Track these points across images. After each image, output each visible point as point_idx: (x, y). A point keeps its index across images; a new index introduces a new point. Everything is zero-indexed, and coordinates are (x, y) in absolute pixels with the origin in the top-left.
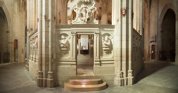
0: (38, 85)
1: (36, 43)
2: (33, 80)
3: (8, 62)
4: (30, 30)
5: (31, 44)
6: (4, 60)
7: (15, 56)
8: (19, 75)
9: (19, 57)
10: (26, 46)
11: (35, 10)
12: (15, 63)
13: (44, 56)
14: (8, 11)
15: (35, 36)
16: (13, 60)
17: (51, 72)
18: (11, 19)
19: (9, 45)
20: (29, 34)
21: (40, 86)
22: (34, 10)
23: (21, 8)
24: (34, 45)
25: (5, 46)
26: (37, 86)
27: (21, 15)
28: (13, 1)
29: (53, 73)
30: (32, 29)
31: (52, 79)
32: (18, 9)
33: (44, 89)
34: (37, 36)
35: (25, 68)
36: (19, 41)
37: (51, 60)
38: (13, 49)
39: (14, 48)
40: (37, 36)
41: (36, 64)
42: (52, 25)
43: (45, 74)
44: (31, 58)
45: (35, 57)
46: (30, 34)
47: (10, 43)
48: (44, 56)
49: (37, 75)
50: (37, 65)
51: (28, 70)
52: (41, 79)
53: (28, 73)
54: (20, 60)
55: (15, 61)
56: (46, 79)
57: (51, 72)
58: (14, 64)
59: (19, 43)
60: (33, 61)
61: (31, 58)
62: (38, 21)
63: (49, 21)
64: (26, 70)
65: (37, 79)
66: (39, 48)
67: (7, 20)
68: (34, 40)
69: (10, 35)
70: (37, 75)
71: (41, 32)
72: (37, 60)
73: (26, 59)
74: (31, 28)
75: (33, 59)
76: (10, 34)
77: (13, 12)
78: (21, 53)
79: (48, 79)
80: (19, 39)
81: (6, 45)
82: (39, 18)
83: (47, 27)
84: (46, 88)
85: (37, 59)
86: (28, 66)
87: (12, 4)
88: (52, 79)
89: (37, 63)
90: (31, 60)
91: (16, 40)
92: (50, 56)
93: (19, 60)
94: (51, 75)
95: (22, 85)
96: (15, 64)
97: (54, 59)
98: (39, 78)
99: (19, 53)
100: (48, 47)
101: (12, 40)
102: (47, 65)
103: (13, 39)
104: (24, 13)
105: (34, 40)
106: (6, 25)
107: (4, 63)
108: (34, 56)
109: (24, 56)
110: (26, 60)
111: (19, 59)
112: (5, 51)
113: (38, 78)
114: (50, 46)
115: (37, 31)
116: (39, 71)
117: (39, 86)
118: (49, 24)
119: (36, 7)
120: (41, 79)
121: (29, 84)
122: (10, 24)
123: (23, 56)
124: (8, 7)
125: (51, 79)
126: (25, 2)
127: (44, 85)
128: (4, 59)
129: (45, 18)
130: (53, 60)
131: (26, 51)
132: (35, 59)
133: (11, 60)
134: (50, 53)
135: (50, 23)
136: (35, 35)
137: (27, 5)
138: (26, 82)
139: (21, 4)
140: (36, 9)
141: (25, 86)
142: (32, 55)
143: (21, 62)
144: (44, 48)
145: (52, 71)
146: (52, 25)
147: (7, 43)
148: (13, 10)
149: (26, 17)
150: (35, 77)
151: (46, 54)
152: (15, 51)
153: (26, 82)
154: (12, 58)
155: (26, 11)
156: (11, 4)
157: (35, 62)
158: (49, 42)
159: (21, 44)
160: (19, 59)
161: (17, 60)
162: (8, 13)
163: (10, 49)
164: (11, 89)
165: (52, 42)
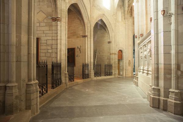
0: (152, 106)
1: (148, 50)
2: (144, 98)
3: (95, 74)
4: (140, 37)
5: (142, 53)
6: (105, 73)
7: (119, 69)
8: (124, 90)
9: (124, 70)
10: (134, 57)
11: (147, 11)
12: (119, 76)
13: (161, 66)
14: (109, 21)
15: (147, 41)
16: (117, 72)
17: (177, 91)
18: (113, 29)
19: (111, 57)
20: (137, 41)
21: (156, 108)
22: (144, 11)
23: (126, 15)
24: (145, 53)
25: (106, 58)
26: (150, 106)
27: (127, 22)
28: (115, 11)
29: (181, 93)
30: (142, 35)
31: (178, 102)
32: (122, 17)
33: (162, 112)
34: (151, 40)
35: (132, 83)
36: (124, 52)
37: (176, 73)
38: (117, 60)
39: (118, 60)
40: (150, 41)
41: (150, 78)
42: (178, 19)
43: (164, 92)
44: (141, 70)
45: (148, 69)
46: (139, 41)
47: (112, 54)
48: (161, 66)
49: (150, 92)
50: (151, 79)
51: (138, 86)
52: (157, 97)
53: (137, 90)
54: (125, 73)
55: (119, 74)
56: (165, 99)
57: (177, 91)
58: (117, 77)
59: (124, 54)
60: (145, 74)
61: (141, 70)
62: (151, 20)
63: (170, 16)
64: (134, 86)
65: (150, 97)
66: (153, 56)
67: (108, 30)
68: (146, 47)
69: (113, 45)
70: (150, 92)
71: (157, 34)
72: (150, 72)
73: (134, 73)
74: (140, 33)
75: (145, 71)
76: (112, 44)
77: (116, 21)
78: (127, 65)
79: (169, 100)
80: (125, 49)
81: (107, 56)
82: (152, 16)
83: (167, 24)
84: (164, 112)
85: (150, 71)
86: (138, 80)
87: (115, 14)
88: (178, 102)
89: (150, 76)
90: (141, 73)
91: (120, 50)
92: (173, 67)
93: (124, 74)
94: (175, 95)
95: (128, 101)
96: (119, 77)
97: (181, 71)
98: (154, 95)
99: (125, 65)
100: (170, 54)
101: (115, 49)
102: (167, 80)
103: (117, 49)
104: (131, 20)
105: (146, 47)
106: (107, 35)
107: (105, 76)
108: (147, 67)
109: (131, 69)
110: (134, 74)
111: (124, 72)
112: (106, 63)
113: (151, 96)
114: (173, 52)
115: (149, 34)
116: (153, 87)
117: (153, 107)
118: (170, 20)
119: (148, 6)
120: (157, 97)
121: (138, 102)
122: (111, 34)
123: (130, 69)
124: (109, 18)
125: (175, 100)
126: (132, 7)
127: (161, 107)
128: (105, 71)
129: (163, 13)
130: (179, 73)
131: (134, 63)
132: (148, 71)
133: (113, 73)
134: (173, 62)
135: (173, 19)
136: (147, 40)
137: (134, 11)
138: (134, 99)
139: (126, 11)
140: (148, 9)
141: (132, 103)
142: (142, 67)
143: (127, 76)
144: (163, 55)
145: (177, 88)
146: (178, 19)
147: (109, 54)
148: (116, 19)
149: (134, 24)
150: (147, 94)
151: (166, 63)
152: (119, 63)
153: (134, 99)
154: (115, 71)
155: (134, 18)
156: (113, 14)
157: (147, 75)
158: (171, 46)
159: (127, 55)
160: (124, 72)
161: (121, 73)
162: (110, 23)
163: (112, 60)
164: (112, 104)
165: (177, 44)
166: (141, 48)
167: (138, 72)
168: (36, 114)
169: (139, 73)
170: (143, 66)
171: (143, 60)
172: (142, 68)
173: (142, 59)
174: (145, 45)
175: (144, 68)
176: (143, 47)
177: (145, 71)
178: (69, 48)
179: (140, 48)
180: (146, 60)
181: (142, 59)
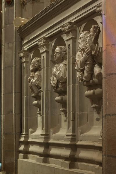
15: (73, 19)
68: (61, 42)
108: (39, 131)
166: (30, 50)
167: (17, 157)
168: (3, 116)
169: (20, 159)
170: (47, 130)
171: (43, 102)
172: (37, 134)
173: (38, 97)
174: (61, 32)
175: (52, 136)
176: (46, 45)
177: (32, 148)
178: (69, 167)
179: (26, 48)
180: (38, 106)
181: (38, 97)
